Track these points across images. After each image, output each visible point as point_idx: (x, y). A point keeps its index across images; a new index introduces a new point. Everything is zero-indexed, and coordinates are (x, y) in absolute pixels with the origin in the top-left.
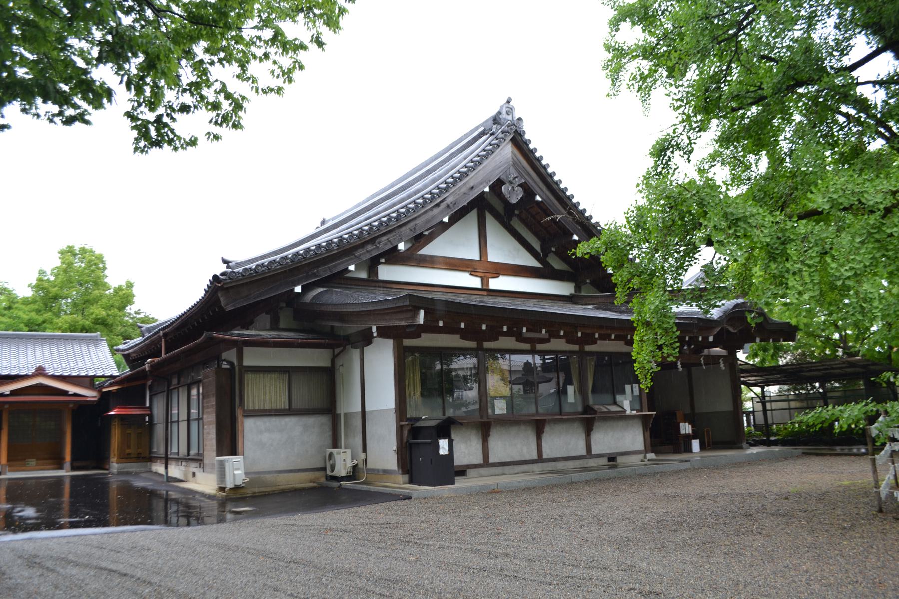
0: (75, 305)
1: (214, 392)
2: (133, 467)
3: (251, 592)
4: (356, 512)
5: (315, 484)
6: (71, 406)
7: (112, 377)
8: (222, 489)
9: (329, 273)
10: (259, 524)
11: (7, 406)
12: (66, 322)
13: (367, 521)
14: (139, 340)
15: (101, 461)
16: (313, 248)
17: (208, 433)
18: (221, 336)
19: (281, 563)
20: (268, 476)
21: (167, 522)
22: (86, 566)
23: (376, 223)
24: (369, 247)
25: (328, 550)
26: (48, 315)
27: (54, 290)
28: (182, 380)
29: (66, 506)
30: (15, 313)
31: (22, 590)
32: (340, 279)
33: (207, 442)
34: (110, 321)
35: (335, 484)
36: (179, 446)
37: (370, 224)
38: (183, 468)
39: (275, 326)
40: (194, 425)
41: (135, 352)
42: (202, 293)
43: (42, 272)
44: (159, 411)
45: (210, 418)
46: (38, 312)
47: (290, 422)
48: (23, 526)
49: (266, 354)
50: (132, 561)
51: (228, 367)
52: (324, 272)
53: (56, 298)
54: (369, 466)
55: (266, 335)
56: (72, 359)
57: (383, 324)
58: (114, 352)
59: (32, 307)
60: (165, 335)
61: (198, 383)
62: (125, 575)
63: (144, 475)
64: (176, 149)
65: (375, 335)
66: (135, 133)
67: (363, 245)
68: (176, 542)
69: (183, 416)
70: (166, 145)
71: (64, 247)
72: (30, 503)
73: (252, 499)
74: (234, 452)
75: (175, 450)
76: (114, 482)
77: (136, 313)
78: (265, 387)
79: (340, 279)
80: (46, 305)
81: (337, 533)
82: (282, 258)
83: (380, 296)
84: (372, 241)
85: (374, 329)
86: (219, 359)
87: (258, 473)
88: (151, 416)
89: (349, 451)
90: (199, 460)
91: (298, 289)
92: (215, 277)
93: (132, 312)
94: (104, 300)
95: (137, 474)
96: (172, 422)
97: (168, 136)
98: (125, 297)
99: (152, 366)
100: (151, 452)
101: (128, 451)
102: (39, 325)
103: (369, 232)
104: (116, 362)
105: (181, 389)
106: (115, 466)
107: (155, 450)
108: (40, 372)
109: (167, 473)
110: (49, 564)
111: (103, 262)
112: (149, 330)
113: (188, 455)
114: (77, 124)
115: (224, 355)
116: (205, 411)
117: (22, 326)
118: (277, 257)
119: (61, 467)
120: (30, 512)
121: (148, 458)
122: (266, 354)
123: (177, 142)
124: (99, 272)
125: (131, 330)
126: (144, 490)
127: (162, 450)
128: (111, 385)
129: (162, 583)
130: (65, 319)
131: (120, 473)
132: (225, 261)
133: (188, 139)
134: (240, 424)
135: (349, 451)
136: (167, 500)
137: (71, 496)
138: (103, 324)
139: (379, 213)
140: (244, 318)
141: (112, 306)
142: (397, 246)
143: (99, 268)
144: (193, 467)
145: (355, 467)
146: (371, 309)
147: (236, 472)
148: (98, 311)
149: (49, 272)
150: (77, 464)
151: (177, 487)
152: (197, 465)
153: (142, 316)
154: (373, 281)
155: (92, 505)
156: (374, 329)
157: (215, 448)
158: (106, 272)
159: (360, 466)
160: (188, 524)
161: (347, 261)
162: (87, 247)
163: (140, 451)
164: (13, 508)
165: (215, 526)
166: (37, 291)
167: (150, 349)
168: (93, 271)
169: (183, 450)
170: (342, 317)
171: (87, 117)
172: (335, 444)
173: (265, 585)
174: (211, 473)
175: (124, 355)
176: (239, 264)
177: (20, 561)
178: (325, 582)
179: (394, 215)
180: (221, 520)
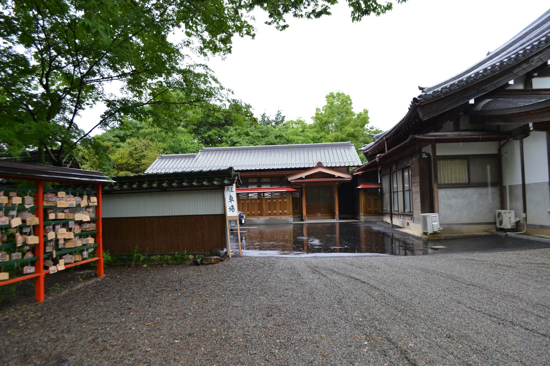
0: (336, 126)
1: (418, 173)
2: (373, 218)
3: (442, 302)
4: (519, 254)
5: (488, 233)
6: (337, 183)
7: (358, 166)
8: (425, 234)
9: (494, 88)
10: (449, 258)
11: (304, 184)
12: (332, 137)
13: (527, 261)
14: (373, 143)
15: (355, 215)
16: (481, 71)
17: (416, 199)
18: (420, 137)
19: (463, 285)
20: (456, 227)
21: (393, 253)
22: (343, 275)
23: (529, 47)
24: (525, 66)
25: (497, 279)
26: (323, 134)
27: (325, 119)
28: (398, 166)
29: (337, 240)
30: (306, 133)
31: (308, 286)
32: (504, 91)
33: (415, 205)
34: (356, 134)
35: (503, 234)
36: (398, 206)
37: (524, 48)
38: (401, 220)
39: (457, 128)
40: (407, 194)
41: (370, 151)
42: (407, 111)
43: (318, 109)
44: (386, 186)
45: (416, 189)
46: (318, 132)
47: (469, 191)
48: (311, 249)
49: (451, 146)
50: (369, 275)
51: (426, 157)
52: (490, 88)
53: (326, 123)
54: (528, 222)
55: (450, 134)
56: (336, 157)
57: (538, 120)
58: (359, 152)
59: (314, 129)
60: (387, 139)
61: (408, 167)
62: (364, 282)
63: (379, 223)
64: (378, 14)
65: (531, 129)
66: (352, 9)
67: (519, 65)
68: (396, 265)
69: (400, 189)
70: (372, 12)
71: (328, 93)
72: (316, 237)
73: (445, 241)
74: (432, 211)
75: (396, 209)
76: (363, 227)
77: (371, 128)
78: (451, 169)
79: (504, 91)
80: (321, 128)
81: (504, 268)
82: (459, 81)
83: (534, 101)
84: (527, 61)
85: (531, 125)
86: (420, 152)
87: (448, 224)
88: (382, 189)
89: (513, 212)
90: (410, 215)
91: (472, 101)
92: (415, 99)
93: (369, 128)
94: (352, 122)
95: (375, 223)
96: (393, 192)
97: (372, 6)
98: (363, 119)
99: (380, 158)
100: (382, 210)
101: (369, 209)
102: (318, 140)
103: (523, 55)
104: (360, 158)
105: (398, 172)
106: (362, 218)
107: (385, 209)
108: (320, 165)
109: (392, 223)
110: (323, 272)
111: (350, 100)
112: (377, 137)
113: (404, 212)
114: (324, 16)
115: (424, 150)
116: (413, 185)
117: (310, 140)
118: (456, 81)
119: (334, 218)
120: (316, 242)
121: (382, 214)
122: (451, 146)
123: (379, 9)
124: (348, 106)
125: (369, 139)
126: (378, 233)
127: (389, 209)
128: (358, 171)
129: (386, 290)
130: (332, 135)
131: (365, 222)
132: (421, 89)
133: (385, 5)
134: (435, 193)
135: (513, 212)
136: (393, 239)
137: (340, 234)
138: (353, 137)
139: (531, 39)
140: (435, 124)
141: (357, 125)
142: (547, 62)
143: (348, 104)
144: (407, 220)
145: (517, 223)
146: (528, 110)
147: (434, 223)
148: (349, 129)
149: (321, 109)
150: (342, 216)
151: (398, 231)
152: (410, 218)
153: (374, 130)
154: (528, 91)
155: (351, 240)
156: (531, 125)
157: (420, 208)
158: (352, 106)
159: (522, 222)
160: (406, 254)
161: (507, 78)
162: (340, 92)
163: (376, 209)
164: (308, 239)
165: (420, 257)
166: (316, 121)
167: (379, 148)
168: (345, 106)
169: (401, 209)
170: (505, 118)
171: (328, 11)
172: (503, 206)
173: (451, 298)
174: (418, 223)
175: (364, 153)
176: (430, 89)
177: (308, 269)
178: (495, 301)
179: (544, 39)
180: (425, 253)
